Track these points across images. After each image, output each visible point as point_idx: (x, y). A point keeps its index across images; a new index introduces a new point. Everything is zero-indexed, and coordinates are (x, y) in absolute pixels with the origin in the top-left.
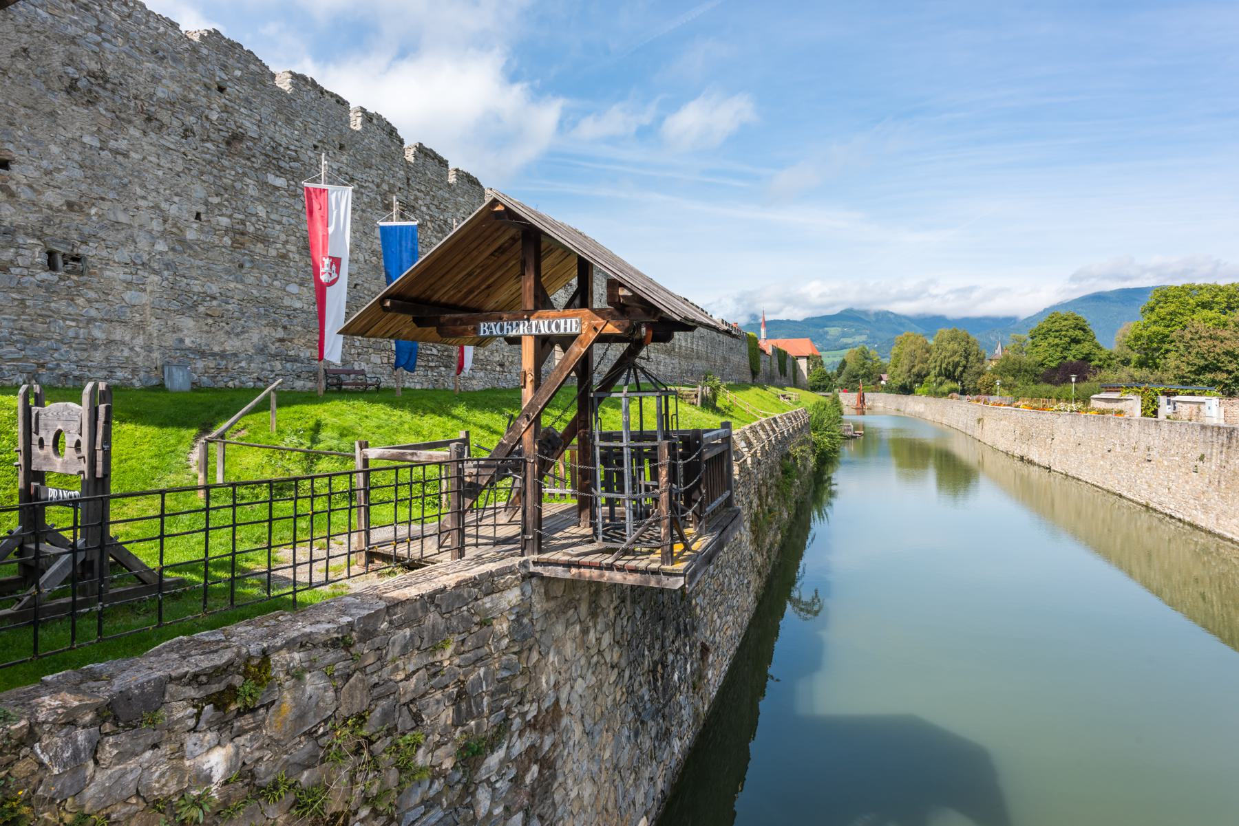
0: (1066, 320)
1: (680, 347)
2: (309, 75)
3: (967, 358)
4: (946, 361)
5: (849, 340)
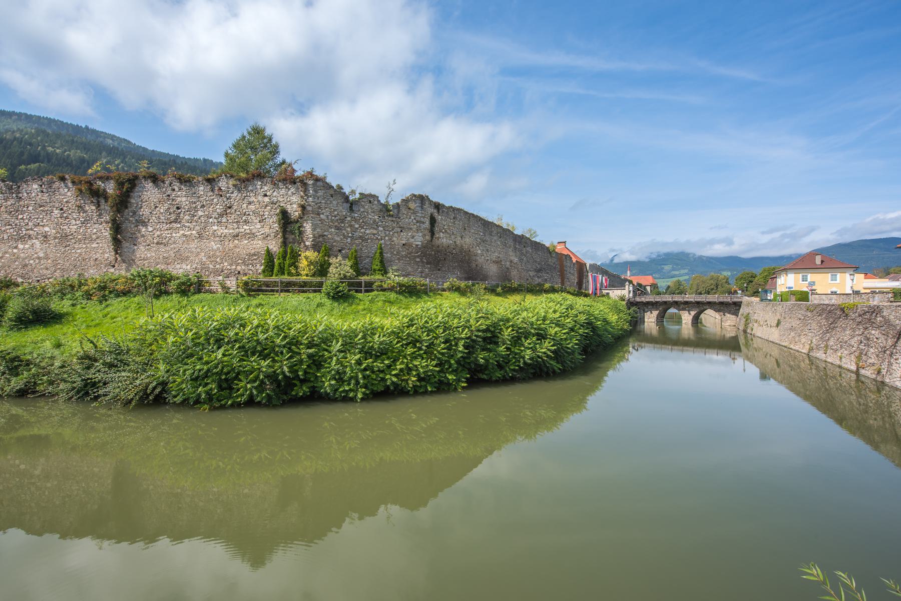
2: (480, 466)
4: (708, 288)
5: (677, 273)
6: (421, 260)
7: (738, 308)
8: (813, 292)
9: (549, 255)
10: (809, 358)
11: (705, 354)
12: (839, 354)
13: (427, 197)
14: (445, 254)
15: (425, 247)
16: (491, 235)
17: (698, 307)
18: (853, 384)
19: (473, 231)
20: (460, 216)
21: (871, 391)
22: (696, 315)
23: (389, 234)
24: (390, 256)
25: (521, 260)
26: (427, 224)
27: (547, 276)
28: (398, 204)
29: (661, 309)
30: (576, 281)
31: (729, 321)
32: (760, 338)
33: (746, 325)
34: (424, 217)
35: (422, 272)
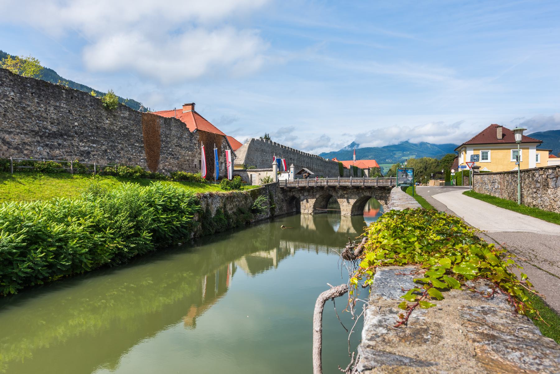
0: (451, 157)
1: (315, 169)
8: (476, 170)
11: (317, 253)
17: (358, 194)
22: (358, 204)
29: (317, 196)
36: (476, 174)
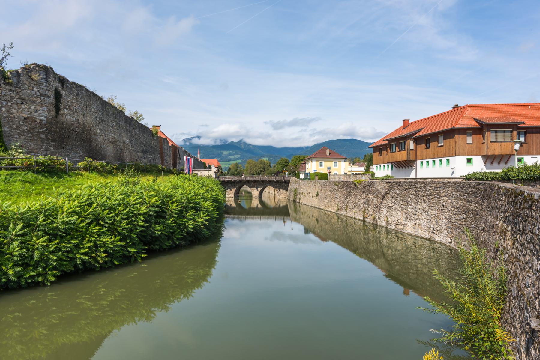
3: (264, 169)
5: (232, 157)
6: (46, 137)
7: (287, 185)
9: (152, 138)
10: (337, 215)
12: (354, 211)
13: (52, 69)
14: (69, 132)
15: (49, 123)
16: (108, 115)
17: (263, 185)
18: (361, 227)
19: (93, 110)
20: (82, 93)
21: (371, 230)
23: (7, 104)
24: (8, 130)
25: (131, 141)
26: (52, 99)
27: (151, 158)
28: (17, 72)
30: (172, 163)
31: (282, 195)
32: (306, 205)
33: (295, 196)
34: (49, 91)
35: (47, 150)
36: (330, 175)
